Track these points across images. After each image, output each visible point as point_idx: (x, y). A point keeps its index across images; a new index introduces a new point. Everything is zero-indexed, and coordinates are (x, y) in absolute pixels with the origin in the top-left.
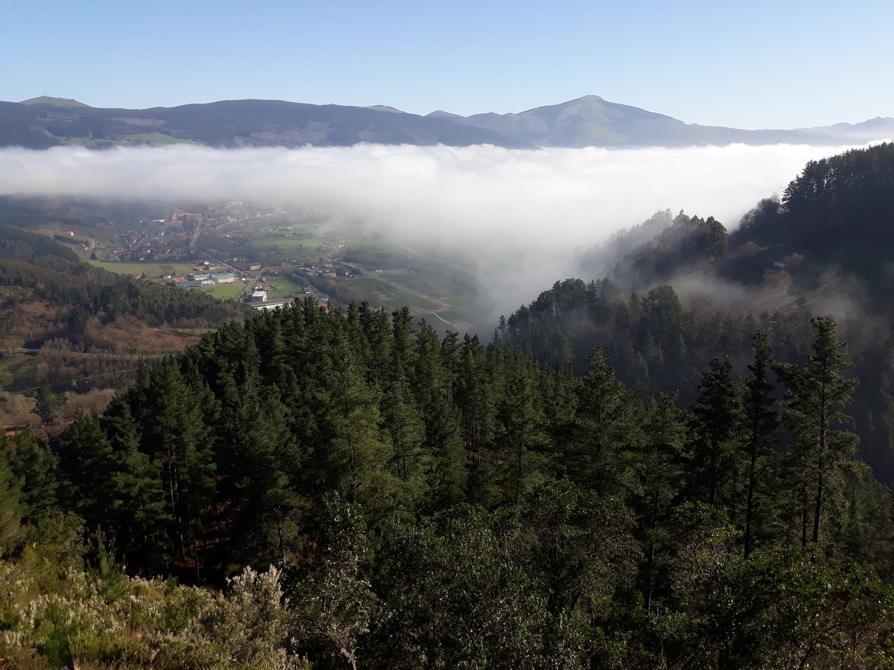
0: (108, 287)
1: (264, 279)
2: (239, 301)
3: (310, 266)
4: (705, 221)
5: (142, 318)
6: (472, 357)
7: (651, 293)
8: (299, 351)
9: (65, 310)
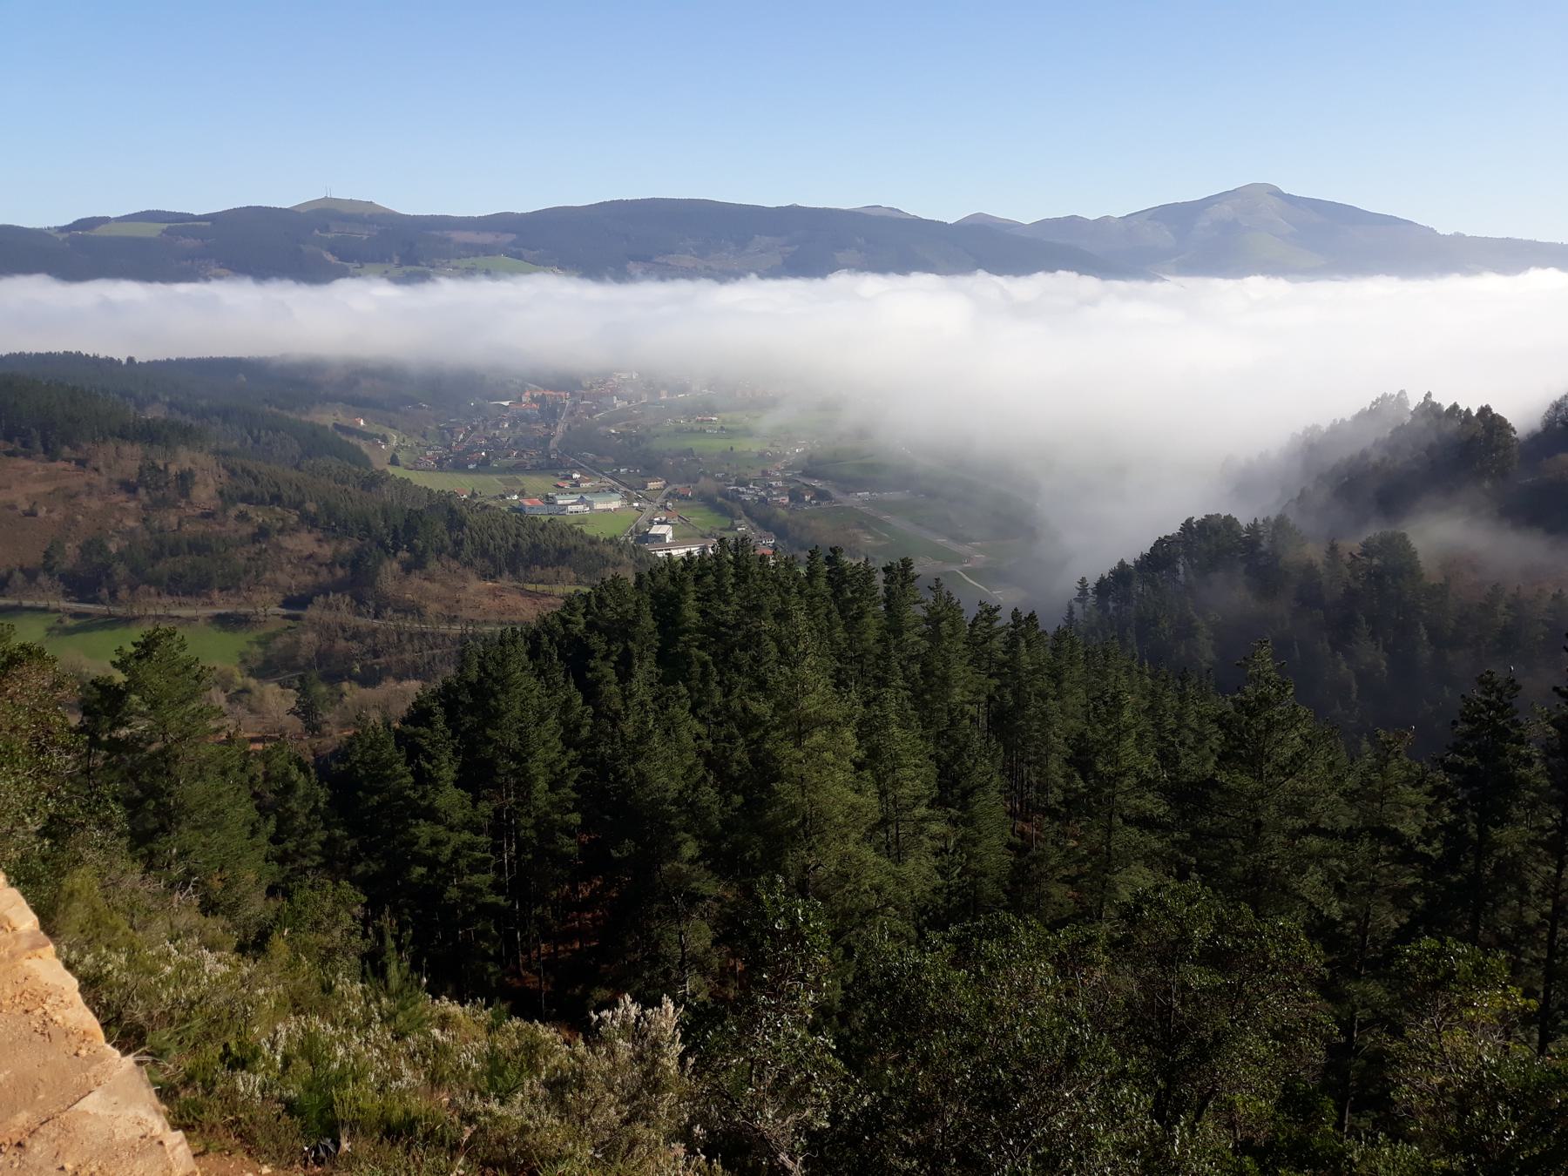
1: (669, 504)
3: (745, 484)
7: (1365, 545)
8: (723, 629)
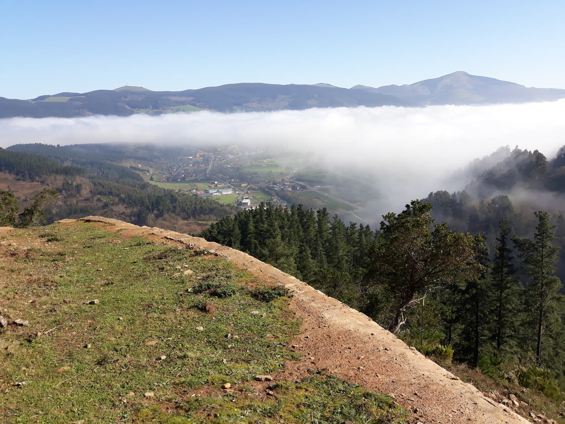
0: (160, 197)
1: (249, 192)
2: (234, 205)
3: (276, 184)
4: (532, 153)
5: (178, 215)
6: (364, 237)
7: (493, 200)
8: (262, 233)
9: (135, 210)
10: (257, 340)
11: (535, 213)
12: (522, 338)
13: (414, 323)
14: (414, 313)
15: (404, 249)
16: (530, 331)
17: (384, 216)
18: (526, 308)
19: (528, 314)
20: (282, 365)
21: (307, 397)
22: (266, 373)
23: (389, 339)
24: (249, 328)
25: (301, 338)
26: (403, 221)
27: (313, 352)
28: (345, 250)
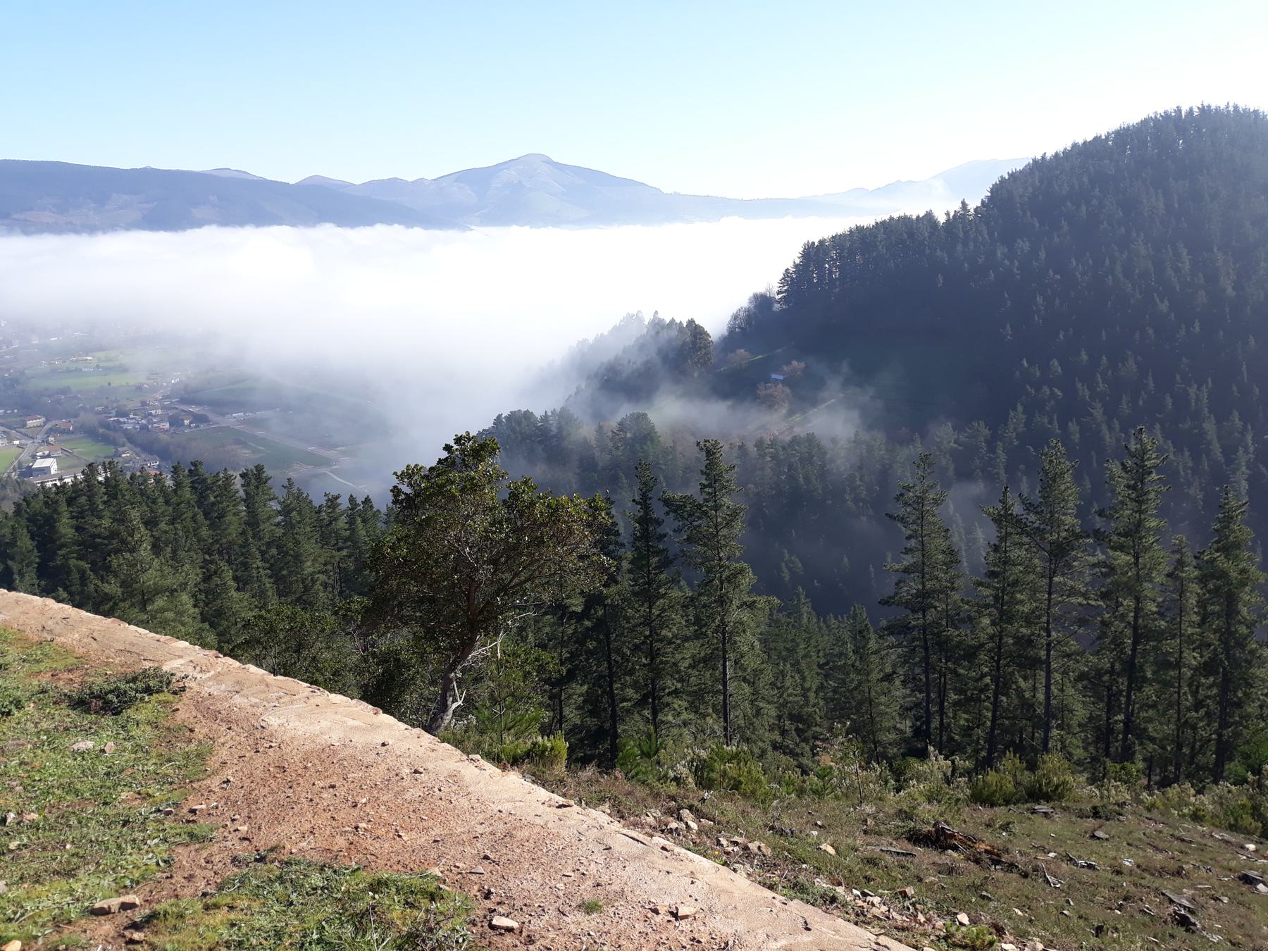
1: (51, 439)
2: (9, 476)
3: (126, 415)
7: (620, 424)
8: (98, 540)
10: (93, 813)
11: (698, 444)
12: (695, 692)
13: (484, 700)
14: (482, 678)
15: (448, 542)
16: (708, 676)
17: (399, 474)
18: (697, 631)
19: (701, 641)
20: (165, 862)
21: (233, 925)
22: (123, 891)
23: (423, 748)
24: (69, 789)
25: (213, 786)
26: (441, 480)
27: (245, 813)
28: (319, 559)
